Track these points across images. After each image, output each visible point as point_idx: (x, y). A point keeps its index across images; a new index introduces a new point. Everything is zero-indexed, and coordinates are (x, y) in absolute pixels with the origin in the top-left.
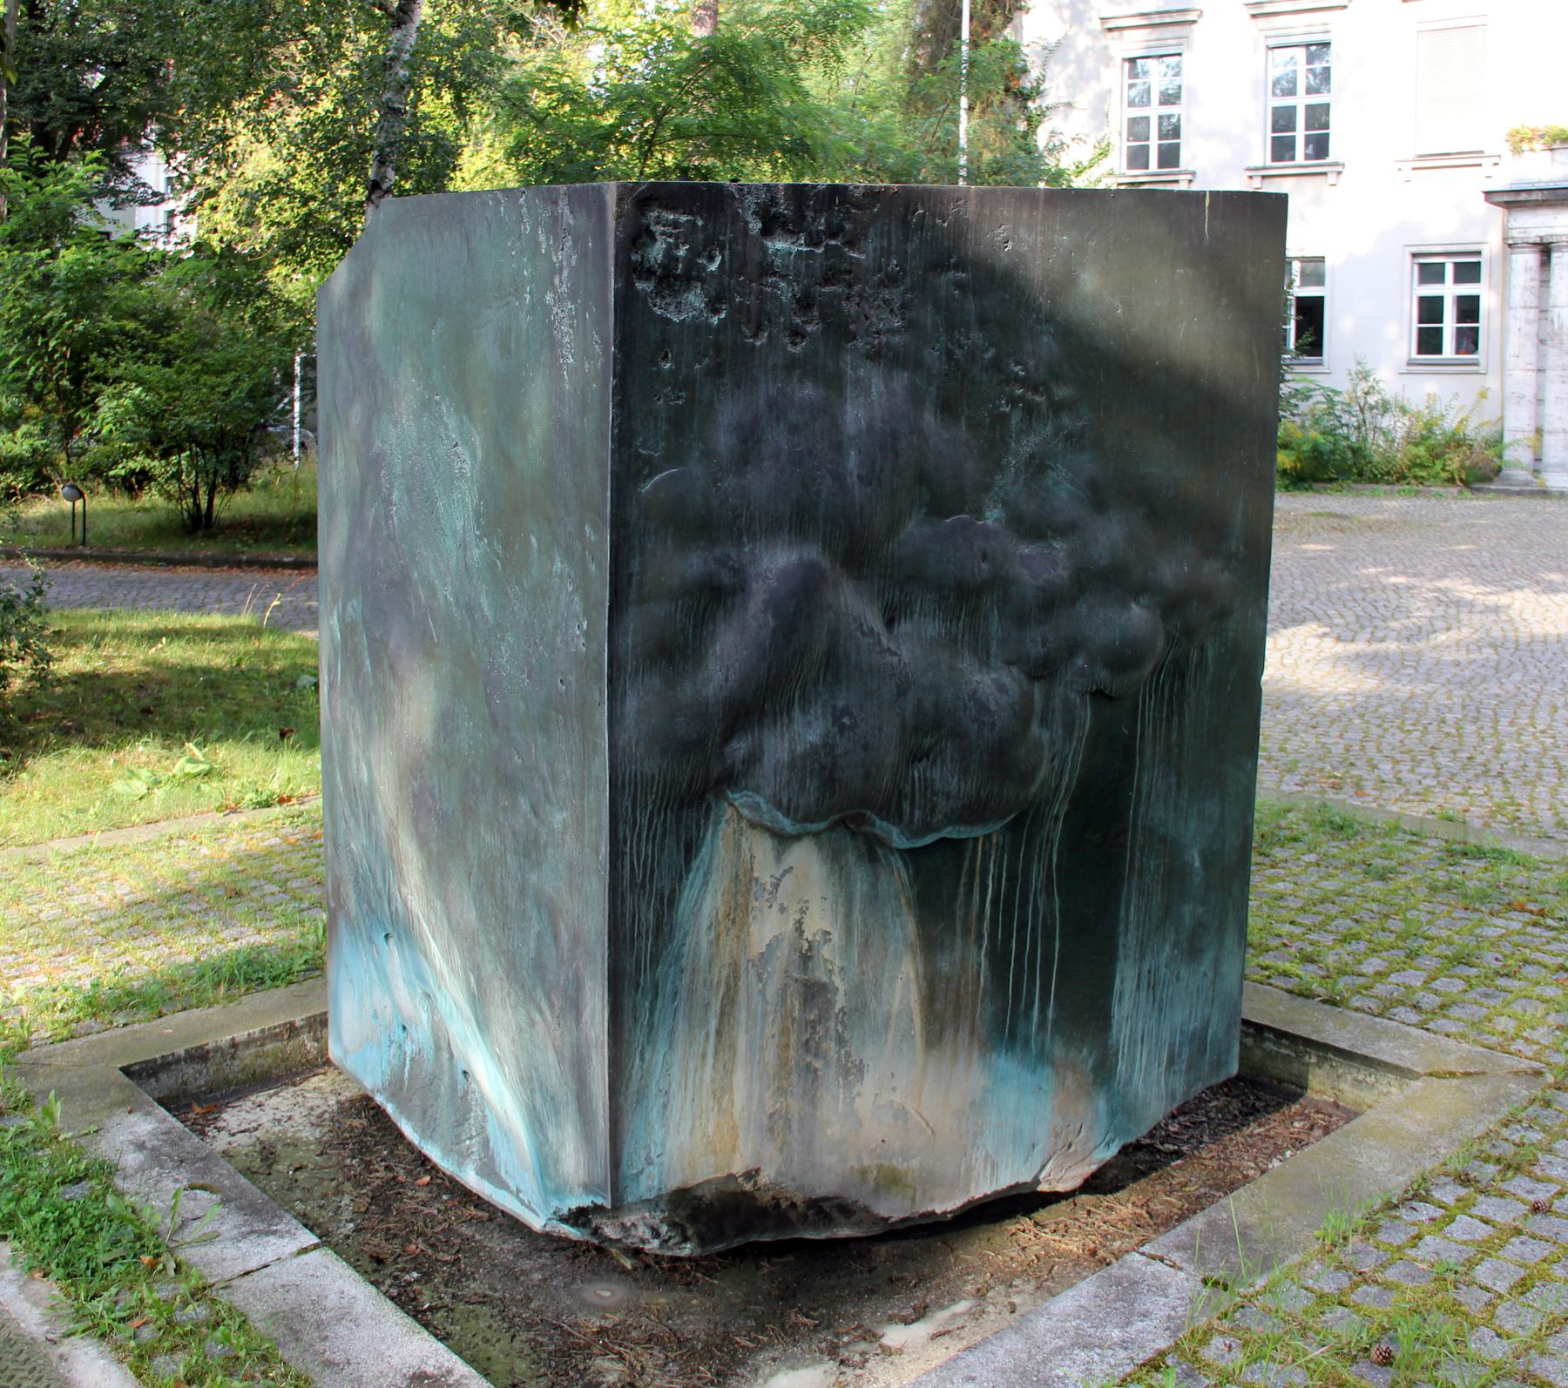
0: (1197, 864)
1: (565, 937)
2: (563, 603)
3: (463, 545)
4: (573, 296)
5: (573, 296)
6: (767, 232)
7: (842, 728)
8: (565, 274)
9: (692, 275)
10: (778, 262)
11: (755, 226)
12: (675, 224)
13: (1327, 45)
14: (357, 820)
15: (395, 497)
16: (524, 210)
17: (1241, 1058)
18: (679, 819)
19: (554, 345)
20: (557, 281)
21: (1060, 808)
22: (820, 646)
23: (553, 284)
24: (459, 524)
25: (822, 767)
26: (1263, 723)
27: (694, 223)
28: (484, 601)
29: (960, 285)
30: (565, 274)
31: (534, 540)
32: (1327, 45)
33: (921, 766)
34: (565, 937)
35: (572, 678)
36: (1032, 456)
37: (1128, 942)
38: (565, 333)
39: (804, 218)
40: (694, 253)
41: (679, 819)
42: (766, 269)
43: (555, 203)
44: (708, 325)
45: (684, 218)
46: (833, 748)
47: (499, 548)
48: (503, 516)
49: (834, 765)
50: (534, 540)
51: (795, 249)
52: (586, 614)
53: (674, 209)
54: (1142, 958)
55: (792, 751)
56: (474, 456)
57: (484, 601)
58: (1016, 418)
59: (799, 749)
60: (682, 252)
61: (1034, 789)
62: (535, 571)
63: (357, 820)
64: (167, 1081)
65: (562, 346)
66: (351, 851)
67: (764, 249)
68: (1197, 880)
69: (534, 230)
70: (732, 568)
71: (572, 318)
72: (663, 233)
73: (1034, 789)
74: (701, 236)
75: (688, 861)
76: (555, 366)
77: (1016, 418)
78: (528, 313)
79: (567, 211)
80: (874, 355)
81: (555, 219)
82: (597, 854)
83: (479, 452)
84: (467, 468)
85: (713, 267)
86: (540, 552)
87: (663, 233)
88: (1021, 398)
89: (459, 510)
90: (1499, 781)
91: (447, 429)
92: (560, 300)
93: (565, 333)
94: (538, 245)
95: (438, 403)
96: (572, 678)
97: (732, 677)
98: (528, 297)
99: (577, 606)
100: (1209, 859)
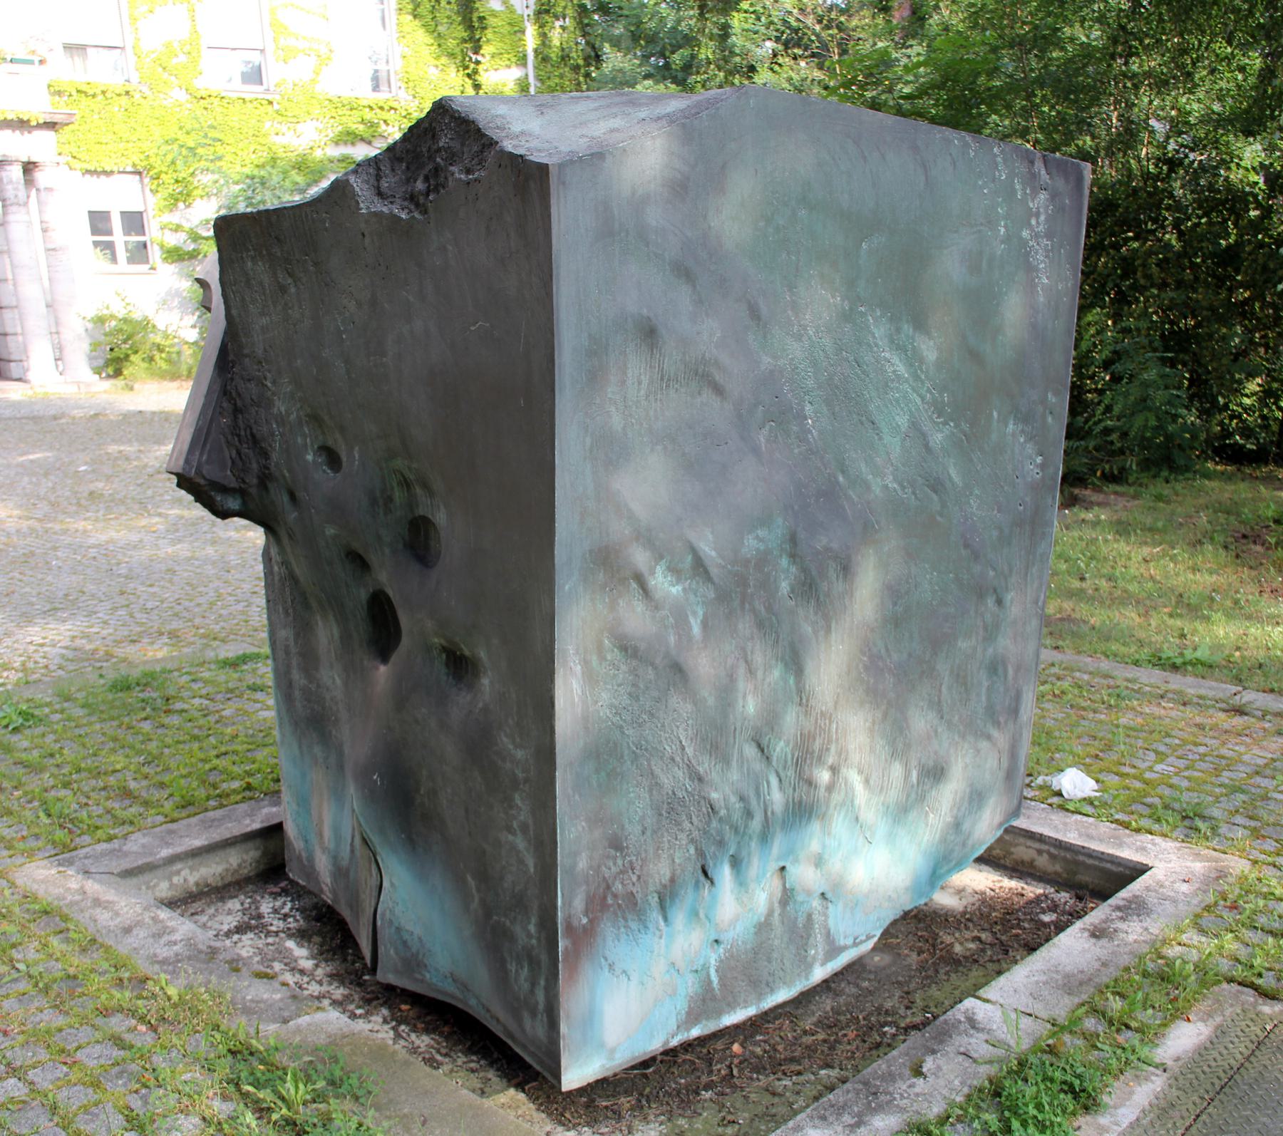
2: (1017, 451)
4: (1049, 235)
5: (1049, 235)
8: (1042, 218)
16: (999, 159)
17: (530, 1067)
19: (1030, 269)
20: (1033, 222)
23: (1029, 224)
26: (215, 249)
30: (1042, 218)
31: (995, 414)
35: (1028, 499)
38: (1040, 260)
43: (1032, 162)
50: (995, 414)
62: (994, 436)
65: (1037, 270)
69: (1010, 177)
71: (1047, 251)
76: (1031, 286)
78: (1002, 242)
79: (1043, 172)
81: (1034, 176)
86: (999, 421)
90: (188, 127)
91: (874, 337)
93: (1040, 260)
94: (1014, 191)
95: (863, 314)
96: (1028, 499)
98: (1003, 230)
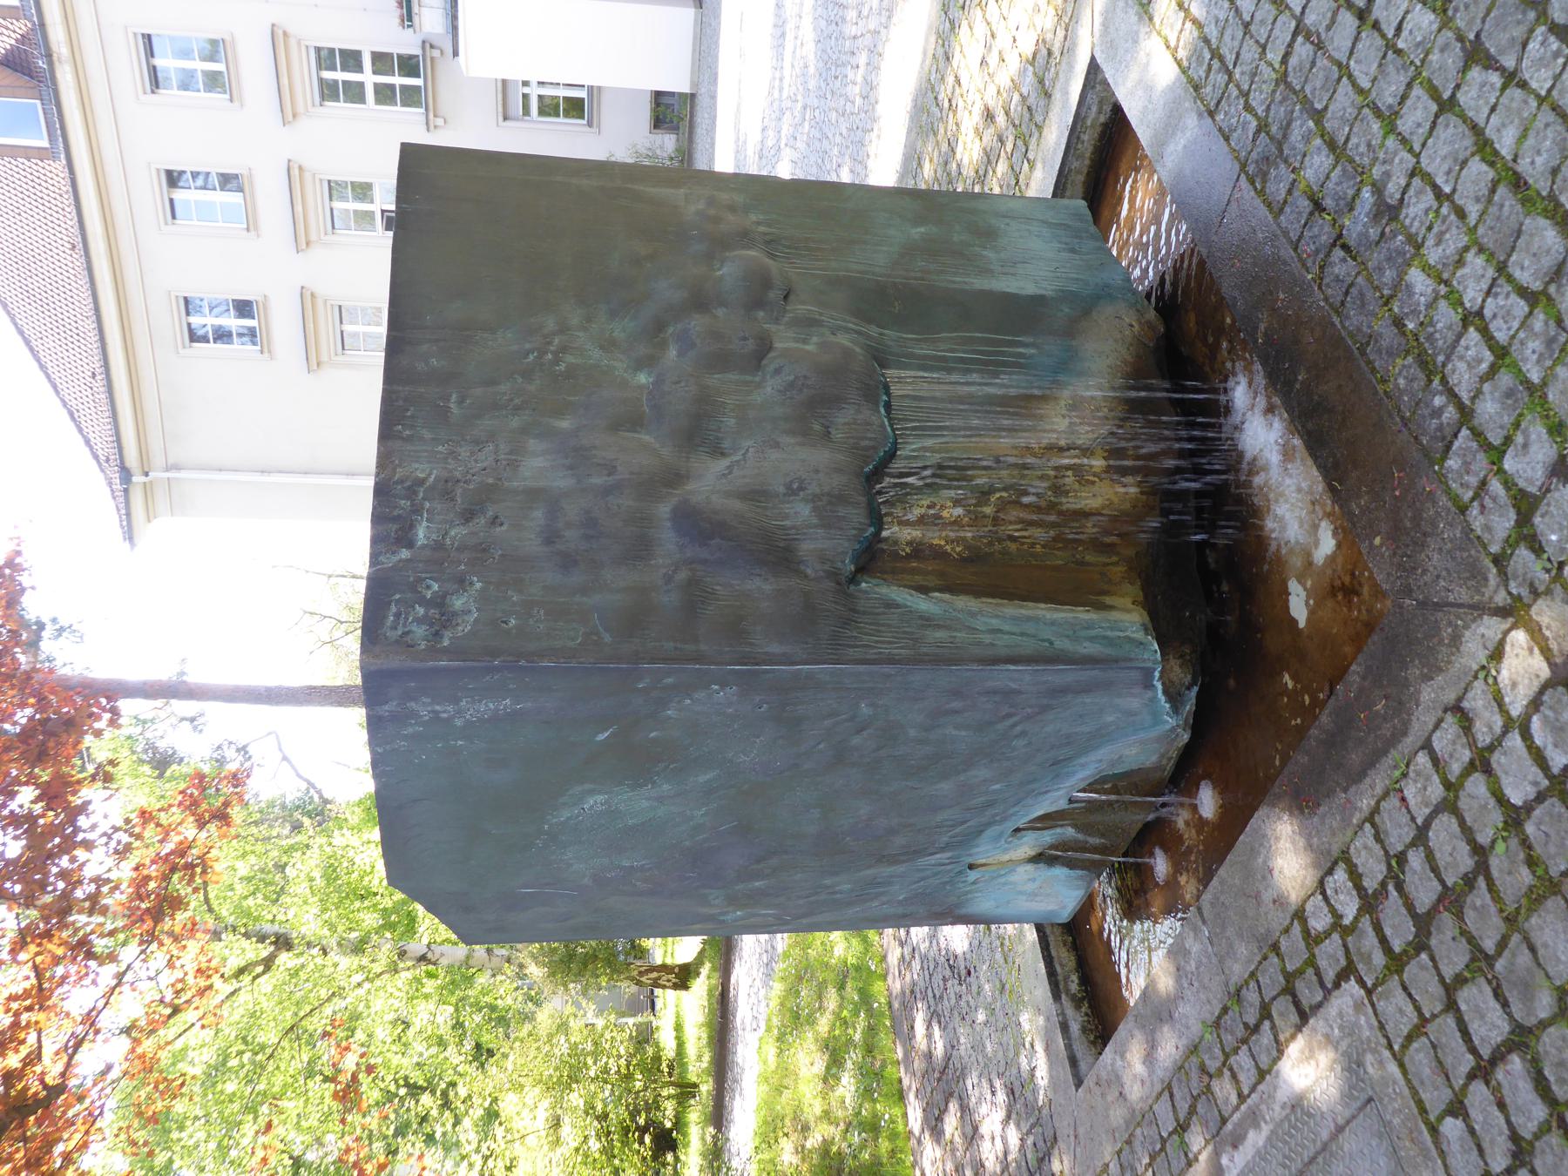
0: (923, 230)
1: (956, 705)
3: (660, 799)
4: (456, 701)
5: (456, 701)
6: (410, 545)
7: (801, 489)
8: (438, 708)
9: (440, 602)
10: (434, 536)
11: (405, 554)
12: (398, 615)
13: (186, 300)
14: (881, 894)
15: (626, 863)
18: (864, 613)
21: (873, 331)
22: (736, 505)
24: (645, 804)
25: (830, 503)
27: (397, 601)
28: (702, 779)
29: (461, 402)
30: (438, 708)
32: (186, 300)
33: (833, 431)
34: (956, 705)
35: (758, 699)
36: (602, 347)
37: (980, 283)
39: (399, 516)
40: (422, 601)
41: (864, 613)
42: (438, 546)
44: (483, 590)
45: (394, 609)
46: (815, 496)
47: (661, 765)
48: (637, 761)
49: (828, 494)
51: (425, 524)
52: (707, 687)
53: (385, 617)
54: (992, 271)
55: (816, 526)
56: (592, 792)
57: (702, 779)
58: (570, 359)
59: (815, 521)
60: (421, 611)
61: (858, 350)
63: (881, 894)
64: (1081, 1048)
66: (906, 899)
67: (424, 547)
68: (934, 229)
70: (675, 572)
72: (405, 625)
73: (858, 350)
74: (409, 595)
75: (898, 606)
77: (570, 359)
80: (514, 465)
82: (889, 676)
83: (587, 786)
84: (600, 798)
85: (436, 587)
87: (405, 625)
88: (555, 353)
89: (637, 803)
92: (459, 712)
96: (758, 699)
97: (758, 571)
99: (700, 695)
100: (919, 220)
